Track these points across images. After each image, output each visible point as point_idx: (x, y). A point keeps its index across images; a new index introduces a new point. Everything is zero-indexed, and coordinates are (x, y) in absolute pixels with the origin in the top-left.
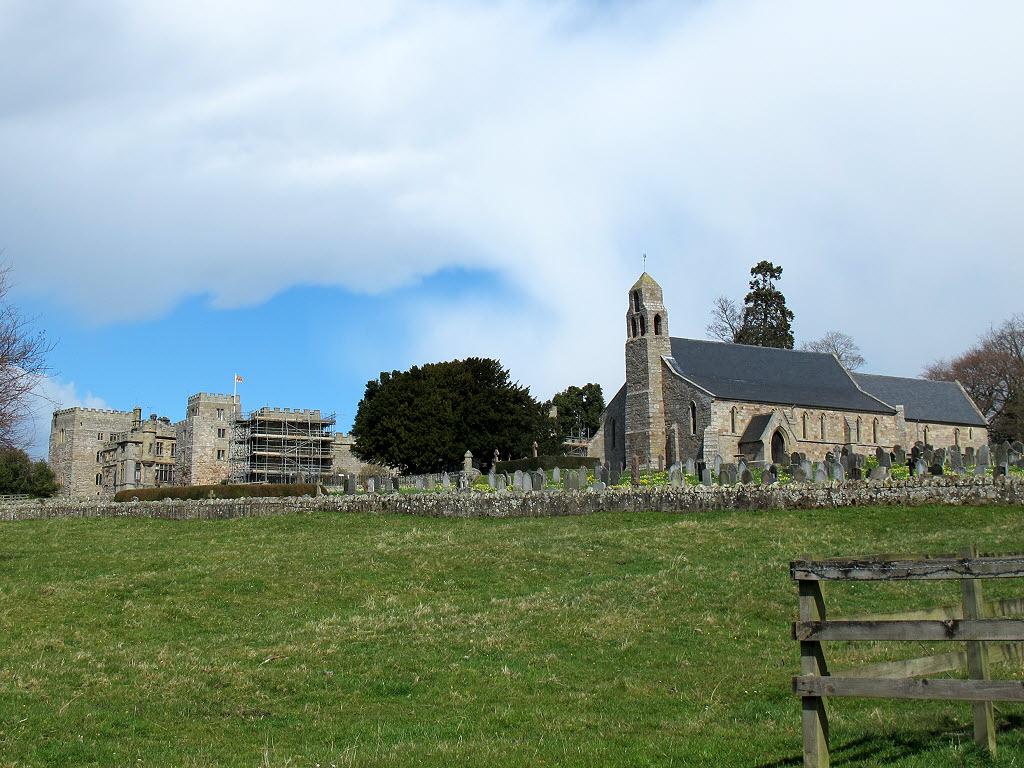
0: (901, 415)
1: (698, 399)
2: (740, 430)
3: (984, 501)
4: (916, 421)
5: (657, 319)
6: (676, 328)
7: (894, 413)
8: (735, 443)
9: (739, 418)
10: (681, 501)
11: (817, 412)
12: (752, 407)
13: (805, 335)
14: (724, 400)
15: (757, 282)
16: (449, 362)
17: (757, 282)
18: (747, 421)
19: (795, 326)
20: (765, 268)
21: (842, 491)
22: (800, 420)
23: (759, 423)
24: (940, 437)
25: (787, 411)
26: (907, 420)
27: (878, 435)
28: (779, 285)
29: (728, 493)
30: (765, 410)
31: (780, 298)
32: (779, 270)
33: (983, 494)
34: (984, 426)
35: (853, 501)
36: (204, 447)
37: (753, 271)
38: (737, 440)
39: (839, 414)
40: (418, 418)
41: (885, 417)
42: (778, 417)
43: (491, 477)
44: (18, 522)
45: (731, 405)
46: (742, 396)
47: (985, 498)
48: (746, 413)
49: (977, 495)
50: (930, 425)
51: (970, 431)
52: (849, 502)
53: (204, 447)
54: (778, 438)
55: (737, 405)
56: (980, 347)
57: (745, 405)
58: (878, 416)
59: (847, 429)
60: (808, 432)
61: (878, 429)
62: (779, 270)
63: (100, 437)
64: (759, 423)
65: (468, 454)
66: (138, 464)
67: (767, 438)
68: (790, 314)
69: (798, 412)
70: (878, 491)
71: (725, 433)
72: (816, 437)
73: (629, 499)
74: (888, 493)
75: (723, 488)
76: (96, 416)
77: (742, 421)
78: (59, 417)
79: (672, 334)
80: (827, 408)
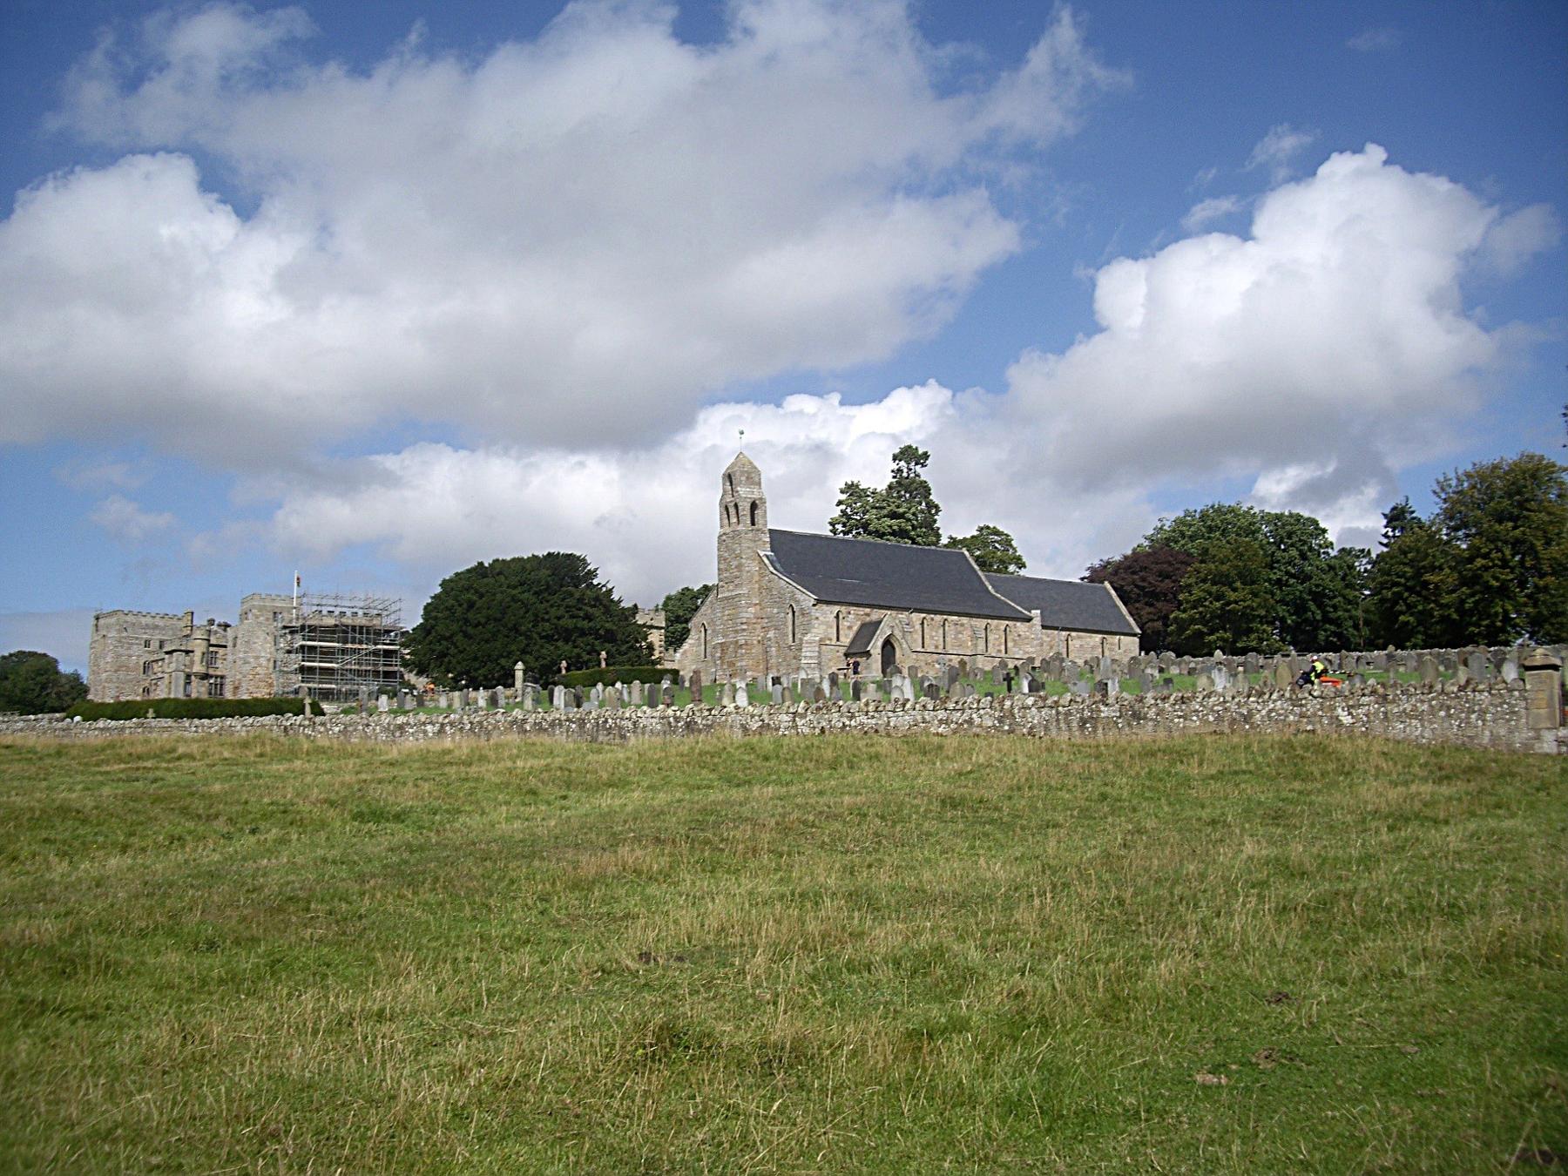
0: (1037, 621)
1: (797, 602)
2: (846, 640)
3: (978, 730)
4: (1056, 628)
5: (754, 506)
6: (777, 518)
7: (1029, 620)
8: (841, 654)
9: (844, 624)
10: (621, 728)
11: (938, 618)
12: (861, 611)
13: (955, 525)
15: (900, 470)
17: (900, 470)
18: (855, 628)
19: (940, 521)
20: (908, 454)
21: (810, 717)
22: (918, 627)
23: (869, 629)
24: (1083, 646)
25: (903, 616)
26: (1044, 627)
27: (1010, 644)
28: (924, 474)
29: (677, 719)
30: (876, 615)
31: (925, 490)
32: (926, 456)
33: (977, 721)
34: (1135, 635)
35: (823, 730)
36: (257, 658)
38: (843, 650)
39: (965, 620)
40: (479, 623)
42: (890, 622)
43: (560, 693)
45: (836, 609)
46: (850, 599)
47: (980, 726)
48: (854, 618)
49: (970, 722)
52: (817, 731)
53: (257, 658)
54: (888, 644)
55: (843, 609)
57: (852, 609)
58: (1011, 623)
59: (975, 637)
62: (926, 456)
63: (147, 644)
64: (869, 629)
65: (520, 665)
66: (188, 676)
67: (876, 647)
68: (937, 507)
69: (916, 617)
70: (852, 717)
73: (561, 725)
74: (864, 719)
75: (670, 712)
76: (143, 620)
77: (850, 628)
78: (102, 621)
79: (770, 527)
80: (993, 618)
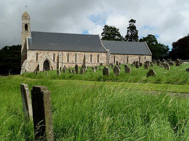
4: (124, 54)
11: (73, 53)
14: (33, 50)
16: (161, 44)
20: (132, 21)
27: (99, 60)
31: (135, 27)
32: (135, 21)
34: (151, 55)
37: (129, 22)
39: (83, 53)
41: (102, 54)
44: (76, 136)
45: (36, 52)
50: (129, 56)
51: (145, 57)
56: (183, 37)
60: (69, 60)
61: (99, 58)
62: (135, 21)
71: (33, 61)
72: (72, 61)
80: (77, 51)
